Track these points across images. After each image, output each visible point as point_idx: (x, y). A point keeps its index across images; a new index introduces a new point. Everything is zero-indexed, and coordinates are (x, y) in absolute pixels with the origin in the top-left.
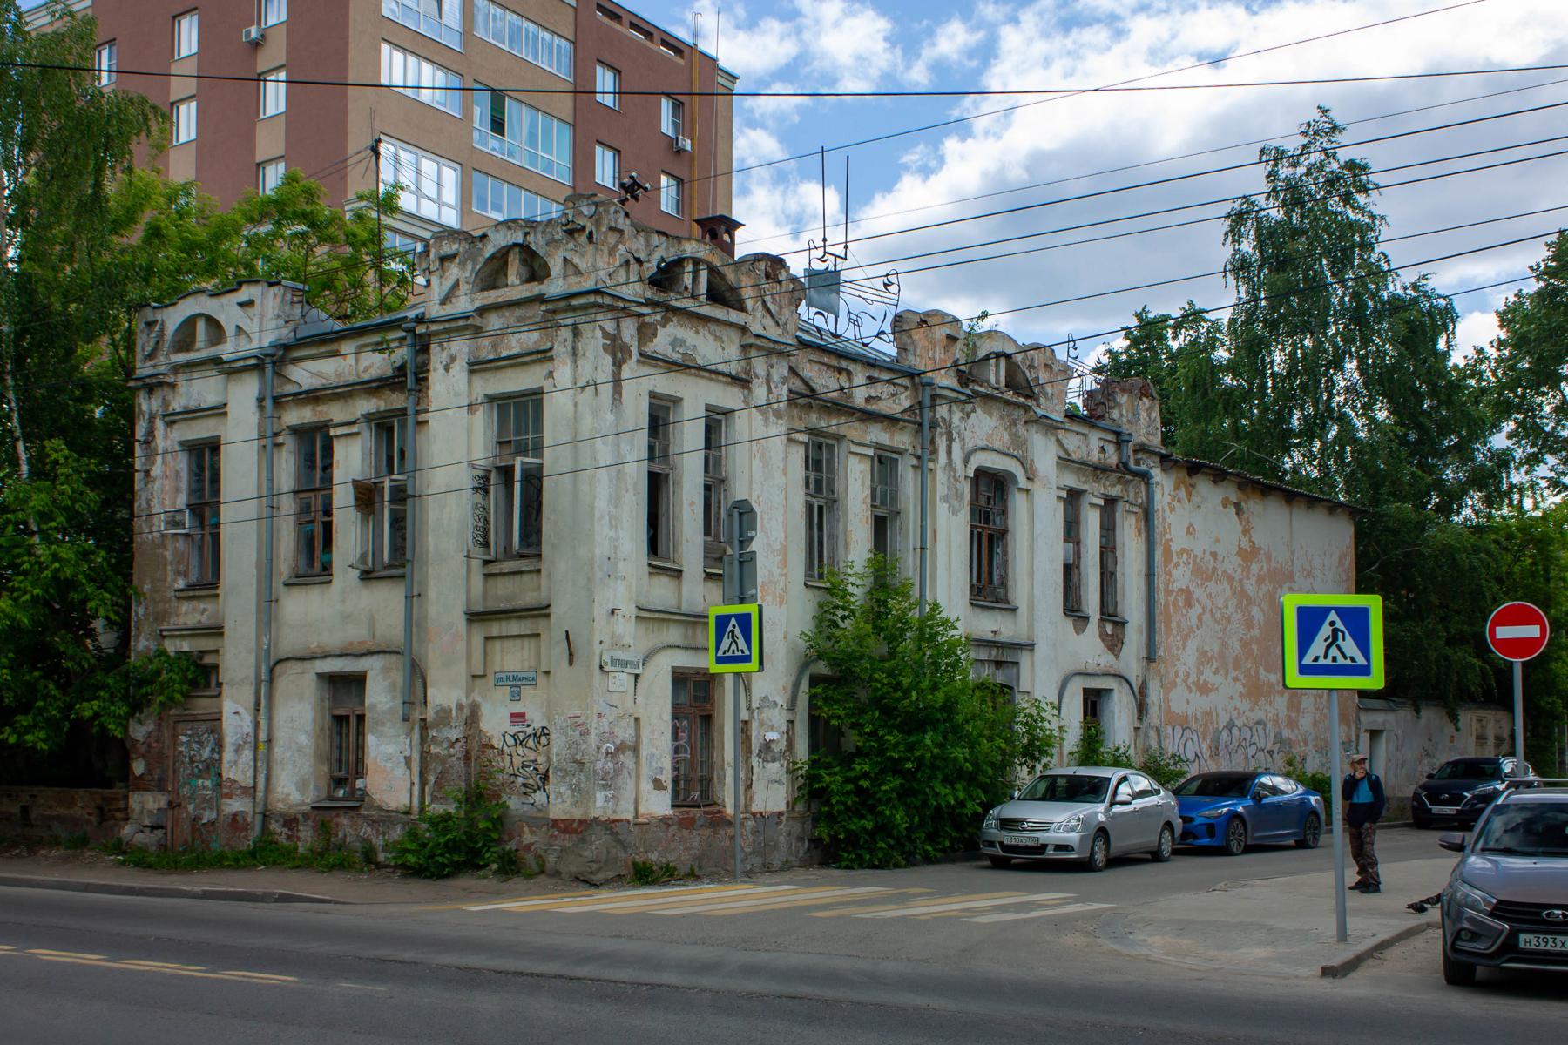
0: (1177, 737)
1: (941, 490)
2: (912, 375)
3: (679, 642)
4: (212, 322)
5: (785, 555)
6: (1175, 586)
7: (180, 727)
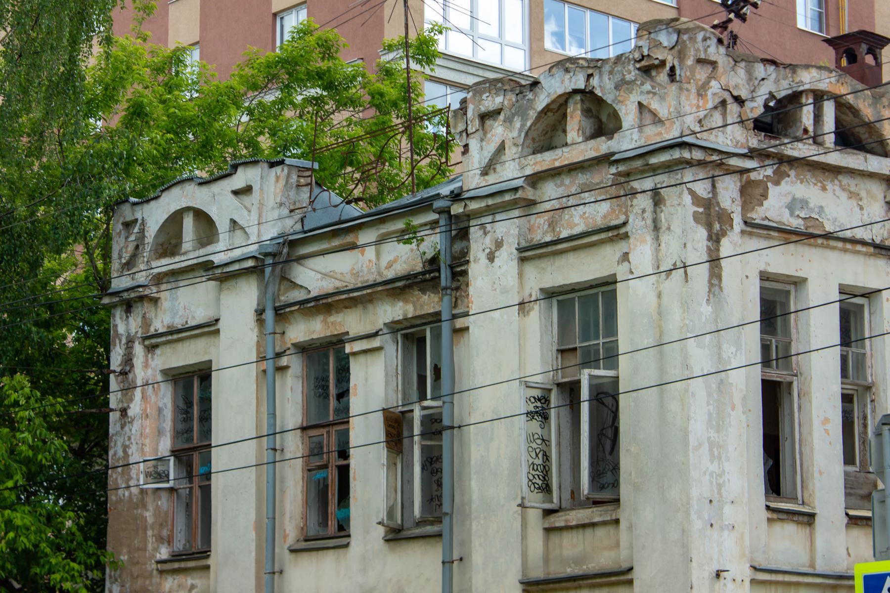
4: (201, 216)
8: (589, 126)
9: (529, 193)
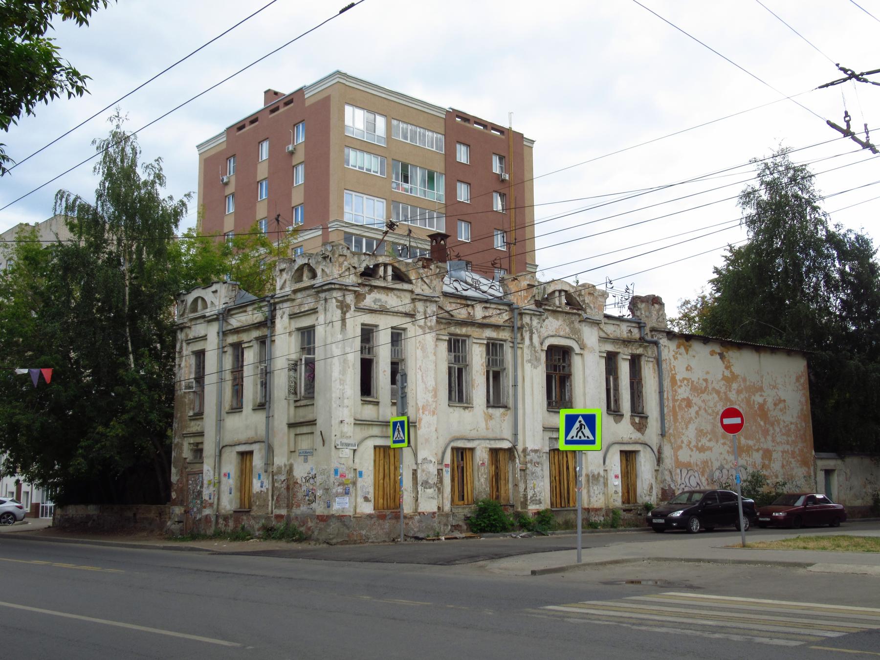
0: (684, 475)
1: (527, 357)
2: (510, 305)
3: (379, 434)
4: (203, 299)
5: (436, 393)
6: (679, 397)
7: (190, 477)
8: (310, 275)
9: (293, 297)
